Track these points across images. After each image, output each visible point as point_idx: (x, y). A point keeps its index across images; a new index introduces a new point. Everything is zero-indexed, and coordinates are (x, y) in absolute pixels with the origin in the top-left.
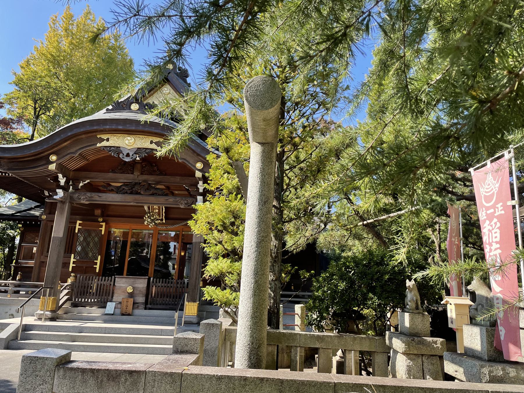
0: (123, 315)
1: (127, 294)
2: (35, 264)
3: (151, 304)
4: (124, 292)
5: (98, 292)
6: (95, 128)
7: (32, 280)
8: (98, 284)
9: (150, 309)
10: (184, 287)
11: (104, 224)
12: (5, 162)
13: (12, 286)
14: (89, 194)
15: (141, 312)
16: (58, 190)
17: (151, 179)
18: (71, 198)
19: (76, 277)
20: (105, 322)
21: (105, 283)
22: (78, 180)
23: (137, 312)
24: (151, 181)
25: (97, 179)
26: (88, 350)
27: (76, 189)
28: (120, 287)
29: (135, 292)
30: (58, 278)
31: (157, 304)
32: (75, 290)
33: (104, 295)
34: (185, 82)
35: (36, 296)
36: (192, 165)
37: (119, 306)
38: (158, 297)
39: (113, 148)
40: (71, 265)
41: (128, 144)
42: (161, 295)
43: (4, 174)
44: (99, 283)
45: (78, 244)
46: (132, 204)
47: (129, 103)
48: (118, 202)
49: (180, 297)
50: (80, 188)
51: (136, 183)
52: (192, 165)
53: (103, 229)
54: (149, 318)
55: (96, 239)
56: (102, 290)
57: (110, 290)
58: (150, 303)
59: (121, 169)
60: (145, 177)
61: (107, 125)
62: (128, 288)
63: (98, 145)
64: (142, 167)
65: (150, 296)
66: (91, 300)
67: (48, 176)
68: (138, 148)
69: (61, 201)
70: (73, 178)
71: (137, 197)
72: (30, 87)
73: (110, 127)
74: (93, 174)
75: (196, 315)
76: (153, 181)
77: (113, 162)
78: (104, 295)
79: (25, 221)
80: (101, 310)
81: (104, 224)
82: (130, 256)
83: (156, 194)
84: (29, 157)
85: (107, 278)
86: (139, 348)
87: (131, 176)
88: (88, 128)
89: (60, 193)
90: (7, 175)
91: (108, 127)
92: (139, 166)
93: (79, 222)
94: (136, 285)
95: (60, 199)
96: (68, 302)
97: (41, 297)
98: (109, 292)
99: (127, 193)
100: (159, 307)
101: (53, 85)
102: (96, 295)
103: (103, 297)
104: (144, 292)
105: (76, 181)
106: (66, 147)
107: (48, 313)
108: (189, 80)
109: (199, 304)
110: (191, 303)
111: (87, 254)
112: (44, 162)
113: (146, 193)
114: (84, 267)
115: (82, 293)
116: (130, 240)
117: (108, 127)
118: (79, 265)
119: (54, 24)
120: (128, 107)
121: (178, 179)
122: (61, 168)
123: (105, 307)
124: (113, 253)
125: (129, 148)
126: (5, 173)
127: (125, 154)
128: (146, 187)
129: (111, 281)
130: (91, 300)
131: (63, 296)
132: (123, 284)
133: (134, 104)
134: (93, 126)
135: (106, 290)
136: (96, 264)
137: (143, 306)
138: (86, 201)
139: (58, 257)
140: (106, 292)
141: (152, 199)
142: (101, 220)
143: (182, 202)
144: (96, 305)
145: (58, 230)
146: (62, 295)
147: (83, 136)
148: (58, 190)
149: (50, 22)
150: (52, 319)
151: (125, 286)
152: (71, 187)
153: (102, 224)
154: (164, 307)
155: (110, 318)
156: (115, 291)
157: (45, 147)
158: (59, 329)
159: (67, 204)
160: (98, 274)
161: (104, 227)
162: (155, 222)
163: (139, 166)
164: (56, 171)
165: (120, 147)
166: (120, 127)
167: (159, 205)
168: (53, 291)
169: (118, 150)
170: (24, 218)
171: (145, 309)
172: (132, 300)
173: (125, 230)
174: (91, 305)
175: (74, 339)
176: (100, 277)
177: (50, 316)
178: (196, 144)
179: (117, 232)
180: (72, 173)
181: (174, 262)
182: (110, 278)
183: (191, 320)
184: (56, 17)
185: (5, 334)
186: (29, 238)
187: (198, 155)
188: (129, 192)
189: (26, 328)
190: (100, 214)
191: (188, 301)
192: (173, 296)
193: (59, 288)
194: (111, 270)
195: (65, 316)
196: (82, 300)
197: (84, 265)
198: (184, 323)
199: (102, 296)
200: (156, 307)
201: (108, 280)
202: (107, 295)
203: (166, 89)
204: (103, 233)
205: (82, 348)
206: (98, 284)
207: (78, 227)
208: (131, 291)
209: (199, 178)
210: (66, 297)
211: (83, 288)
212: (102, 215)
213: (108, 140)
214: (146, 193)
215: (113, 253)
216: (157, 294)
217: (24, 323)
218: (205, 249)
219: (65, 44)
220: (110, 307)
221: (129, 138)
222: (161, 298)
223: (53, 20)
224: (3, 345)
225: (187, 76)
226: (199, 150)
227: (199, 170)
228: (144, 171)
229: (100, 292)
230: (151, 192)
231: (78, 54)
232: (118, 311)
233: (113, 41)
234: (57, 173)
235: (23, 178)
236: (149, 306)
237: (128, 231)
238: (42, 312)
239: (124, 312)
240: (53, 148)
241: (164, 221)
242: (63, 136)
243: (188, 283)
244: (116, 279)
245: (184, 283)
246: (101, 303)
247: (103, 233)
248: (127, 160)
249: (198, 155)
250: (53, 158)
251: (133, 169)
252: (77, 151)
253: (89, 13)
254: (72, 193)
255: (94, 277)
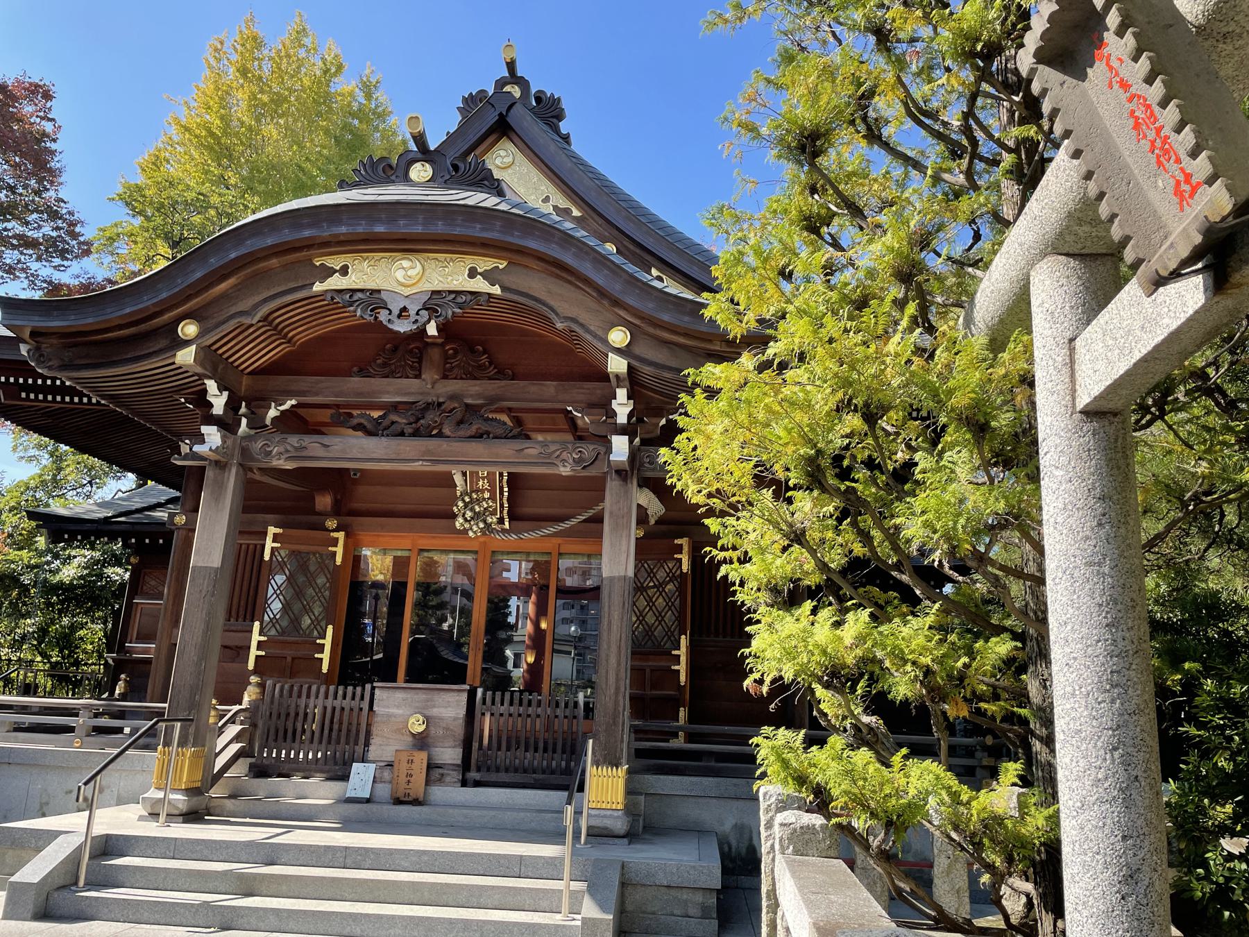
0: (398, 802)
1: (410, 739)
2: (158, 649)
3: (478, 770)
4: (398, 731)
5: (326, 732)
6: (307, 233)
7: (148, 697)
8: (325, 708)
9: (478, 784)
10: (575, 717)
11: (341, 535)
12: (51, 345)
13: (87, 714)
14: (294, 440)
15: (450, 793)
16: (205, 429)
17: (473, 390)
18: (245, 452)
19: (262, 686)
20: (348, 825)
21: (355, 704)
22: (263, 399)
23: (439, 793)
24: (471, 396)
25: (316, 394)
26: (292, 925)
27: (257, 424)
28: (389, 716)
29: (433, 731)
30: (210, 690)
31: (498, 770)
32: (260, 724)
33: (343, 740)
34: (557, 130)
35: (147, 741)
36: (595, 336)
37: (387, 774)
38: (499, 749)
39: (360, 295)
40: (254, 652)
41: (405, 281)
42: (508, 740)
43: (49, 382)
44: (329, 703)
45: (271, 591)
46: (417, 466)
47: (403, 164)
48: (380, 460)
49: (574, 751)
50: (268, 421)
51: (428, 406)
52: (595, 336)
53: (339, 550)
54: (477, 813)
55: (321, 580)
56: (336, 727)
57: (359, 724)
58: (477, 766)
59: (385, 365)
60: (453, 386)
61: (339, 222)
62: (412, 720)
63: (318, 287)
64: (446, 358)
65: (475, 745)
66: (306, 755)
67: (179, 390)
68: (434, 292)
69: (217, 463)
70: (248, 396)
71: (432, 444)
72: (160, 208)
73: (351, 230)
74: (306, 382)
75: (620, 807)
76: (479, 396)
77: (370, 343)
78: (343, 740)
79: (140, 537)
80: (335, 787)
81: (341, 535)
82: (413, 633)
83: (488, 433)
84: (120, 327)
85: (350, 688)
86: (451, 922)
87: (412, 384)
88: (287, 235)
89: (213, 436)
90: (58, 382)
91: (343, 229)
92: (435, 354)
93: (272, 530)
94: (435, 712)
95: (214, 457)
96: (241, 760)
97: (160, 747)
98: (358, 731)
99: (402, 434)
100: (503, 777)
101: (215, 200)
102: (320, 742)
103: (339, 748)
104: (459, 730)
105: (258, 401)
106: (224, 296)
107: (180, 797)
108: (564, 127)
109: (629, 772)
110: (605, 770)
111: (295, 622)
112: (163, 343)
113: (461, 433)
114: (289, 659)
115: (281, 734)
116: (414, 575)
117: (343, 229)
118: (276, 651)
119: (219, 60)
120: (400, 173)
121: (550, 388)
122: (213, 361)
123: (345, 777)
124: (370, 629)
125: (407, 292)
126: (54, 379)
127: (396, 312)
128: (459, 416)
129: (362, 698)
130: (306, 755)
131: (227, 744)
132: (398, 707)
133: (418, 165)
134: (302, 227)
135: (350, 724)
136: (321, 648)
137: (456, 776)
138: (287, 459)
139: (208, 628)
140: (349, 731)
141: (477, 449)
142: (331, 523)
143: (565, 455)
144: (321, 771)
145: (209, 544)
146: (221, 742)
147: (274, 262)
148: (205, 429)
149: (209, 54)
150: (193, 816)
151: (404, 712)
152: (244, 421)
153: (335, 535)
154: (518, 778)
155: (359, 814)
156: (374, 730)
157: (164, 295)
158: (206, 852)
159: (234, 470)
160: (327, 679)
161: (341, 543)
162: (485, 521)
163: (435, 354)
164: (199, 370)
165: (379, 291)
166: (380, 229)
167: (492, 469)
168: (192, 730)
169: (374, 299)
170: (138, 528)
171: (464, 783)
172: (423, 756)
173: (399, 553)
174: (307, 771)
175: (248, 887)
176: (332, 688)
177: (183, 807)
178: (609, 268)
179: (378, 566)
180: (245, 381)
181: (520, 648)
182: (359, 689)
183: (608, 823)
184: (222, 43)
185: (34, 871)
186: (153, 583)
187: (616, 303)
188: (408, 430)
189: (107, 847)
190: (329, 508)
191: (597, 763)
192: (546, 743)
193: (212, 720)
194: (361, 667)
195: (229, 804)
196: (279, 754)
197: (289, 653)
198: (588, 835)
199: (338, 742)
200: (493, 777)
201: (354, 694)
202: (352, 740)
203: (502, 153)
204: (339, 560)
205: (273, 921)
206: (325, 708)
207: (269, 544)
208: (421, 728)
209: (617, 376)
210: (235, 747)
211: (283, 717)
212: (337, 511)
213: (344, 271)
214: (461, 433)
215: (370, 629)
216: (497, 737)
217: (99, 830)
218: (723, 570)
219: (241, 111)
220: (362, 777)
221: (406, 263)
222: (508, 749)
223: (216, 50)
224: (31, 907)
225: (560, 116)
226: (618, 287)
227: (619, 351)
228: (451, 369)
229: (331, 730)
230: (473, 429)
231: (270, 130)
232: (384, 791)
233: (361, 97)
234: (201, 377)
235: (111, 398)
236: (473, 775)
237: (406, 554)
238: (161, 795)
239: (400, 794)
240: (189, 298)
241: (507, 524)
242: (214, 262)
243: (586, 704)
244: (377, 692)
245: (576, 704)
246: (336, 763)
247: (339, 560)
248: (402, 327)
249: (616, 303)
250: (189, 329)
251: (420, 362)
252: (256, 307)
253: (303, 32)
254: (247, 438)
255: (314, 688)
